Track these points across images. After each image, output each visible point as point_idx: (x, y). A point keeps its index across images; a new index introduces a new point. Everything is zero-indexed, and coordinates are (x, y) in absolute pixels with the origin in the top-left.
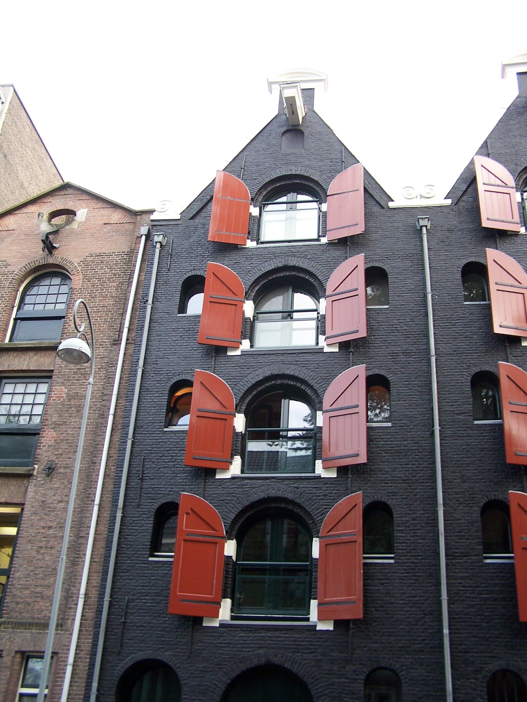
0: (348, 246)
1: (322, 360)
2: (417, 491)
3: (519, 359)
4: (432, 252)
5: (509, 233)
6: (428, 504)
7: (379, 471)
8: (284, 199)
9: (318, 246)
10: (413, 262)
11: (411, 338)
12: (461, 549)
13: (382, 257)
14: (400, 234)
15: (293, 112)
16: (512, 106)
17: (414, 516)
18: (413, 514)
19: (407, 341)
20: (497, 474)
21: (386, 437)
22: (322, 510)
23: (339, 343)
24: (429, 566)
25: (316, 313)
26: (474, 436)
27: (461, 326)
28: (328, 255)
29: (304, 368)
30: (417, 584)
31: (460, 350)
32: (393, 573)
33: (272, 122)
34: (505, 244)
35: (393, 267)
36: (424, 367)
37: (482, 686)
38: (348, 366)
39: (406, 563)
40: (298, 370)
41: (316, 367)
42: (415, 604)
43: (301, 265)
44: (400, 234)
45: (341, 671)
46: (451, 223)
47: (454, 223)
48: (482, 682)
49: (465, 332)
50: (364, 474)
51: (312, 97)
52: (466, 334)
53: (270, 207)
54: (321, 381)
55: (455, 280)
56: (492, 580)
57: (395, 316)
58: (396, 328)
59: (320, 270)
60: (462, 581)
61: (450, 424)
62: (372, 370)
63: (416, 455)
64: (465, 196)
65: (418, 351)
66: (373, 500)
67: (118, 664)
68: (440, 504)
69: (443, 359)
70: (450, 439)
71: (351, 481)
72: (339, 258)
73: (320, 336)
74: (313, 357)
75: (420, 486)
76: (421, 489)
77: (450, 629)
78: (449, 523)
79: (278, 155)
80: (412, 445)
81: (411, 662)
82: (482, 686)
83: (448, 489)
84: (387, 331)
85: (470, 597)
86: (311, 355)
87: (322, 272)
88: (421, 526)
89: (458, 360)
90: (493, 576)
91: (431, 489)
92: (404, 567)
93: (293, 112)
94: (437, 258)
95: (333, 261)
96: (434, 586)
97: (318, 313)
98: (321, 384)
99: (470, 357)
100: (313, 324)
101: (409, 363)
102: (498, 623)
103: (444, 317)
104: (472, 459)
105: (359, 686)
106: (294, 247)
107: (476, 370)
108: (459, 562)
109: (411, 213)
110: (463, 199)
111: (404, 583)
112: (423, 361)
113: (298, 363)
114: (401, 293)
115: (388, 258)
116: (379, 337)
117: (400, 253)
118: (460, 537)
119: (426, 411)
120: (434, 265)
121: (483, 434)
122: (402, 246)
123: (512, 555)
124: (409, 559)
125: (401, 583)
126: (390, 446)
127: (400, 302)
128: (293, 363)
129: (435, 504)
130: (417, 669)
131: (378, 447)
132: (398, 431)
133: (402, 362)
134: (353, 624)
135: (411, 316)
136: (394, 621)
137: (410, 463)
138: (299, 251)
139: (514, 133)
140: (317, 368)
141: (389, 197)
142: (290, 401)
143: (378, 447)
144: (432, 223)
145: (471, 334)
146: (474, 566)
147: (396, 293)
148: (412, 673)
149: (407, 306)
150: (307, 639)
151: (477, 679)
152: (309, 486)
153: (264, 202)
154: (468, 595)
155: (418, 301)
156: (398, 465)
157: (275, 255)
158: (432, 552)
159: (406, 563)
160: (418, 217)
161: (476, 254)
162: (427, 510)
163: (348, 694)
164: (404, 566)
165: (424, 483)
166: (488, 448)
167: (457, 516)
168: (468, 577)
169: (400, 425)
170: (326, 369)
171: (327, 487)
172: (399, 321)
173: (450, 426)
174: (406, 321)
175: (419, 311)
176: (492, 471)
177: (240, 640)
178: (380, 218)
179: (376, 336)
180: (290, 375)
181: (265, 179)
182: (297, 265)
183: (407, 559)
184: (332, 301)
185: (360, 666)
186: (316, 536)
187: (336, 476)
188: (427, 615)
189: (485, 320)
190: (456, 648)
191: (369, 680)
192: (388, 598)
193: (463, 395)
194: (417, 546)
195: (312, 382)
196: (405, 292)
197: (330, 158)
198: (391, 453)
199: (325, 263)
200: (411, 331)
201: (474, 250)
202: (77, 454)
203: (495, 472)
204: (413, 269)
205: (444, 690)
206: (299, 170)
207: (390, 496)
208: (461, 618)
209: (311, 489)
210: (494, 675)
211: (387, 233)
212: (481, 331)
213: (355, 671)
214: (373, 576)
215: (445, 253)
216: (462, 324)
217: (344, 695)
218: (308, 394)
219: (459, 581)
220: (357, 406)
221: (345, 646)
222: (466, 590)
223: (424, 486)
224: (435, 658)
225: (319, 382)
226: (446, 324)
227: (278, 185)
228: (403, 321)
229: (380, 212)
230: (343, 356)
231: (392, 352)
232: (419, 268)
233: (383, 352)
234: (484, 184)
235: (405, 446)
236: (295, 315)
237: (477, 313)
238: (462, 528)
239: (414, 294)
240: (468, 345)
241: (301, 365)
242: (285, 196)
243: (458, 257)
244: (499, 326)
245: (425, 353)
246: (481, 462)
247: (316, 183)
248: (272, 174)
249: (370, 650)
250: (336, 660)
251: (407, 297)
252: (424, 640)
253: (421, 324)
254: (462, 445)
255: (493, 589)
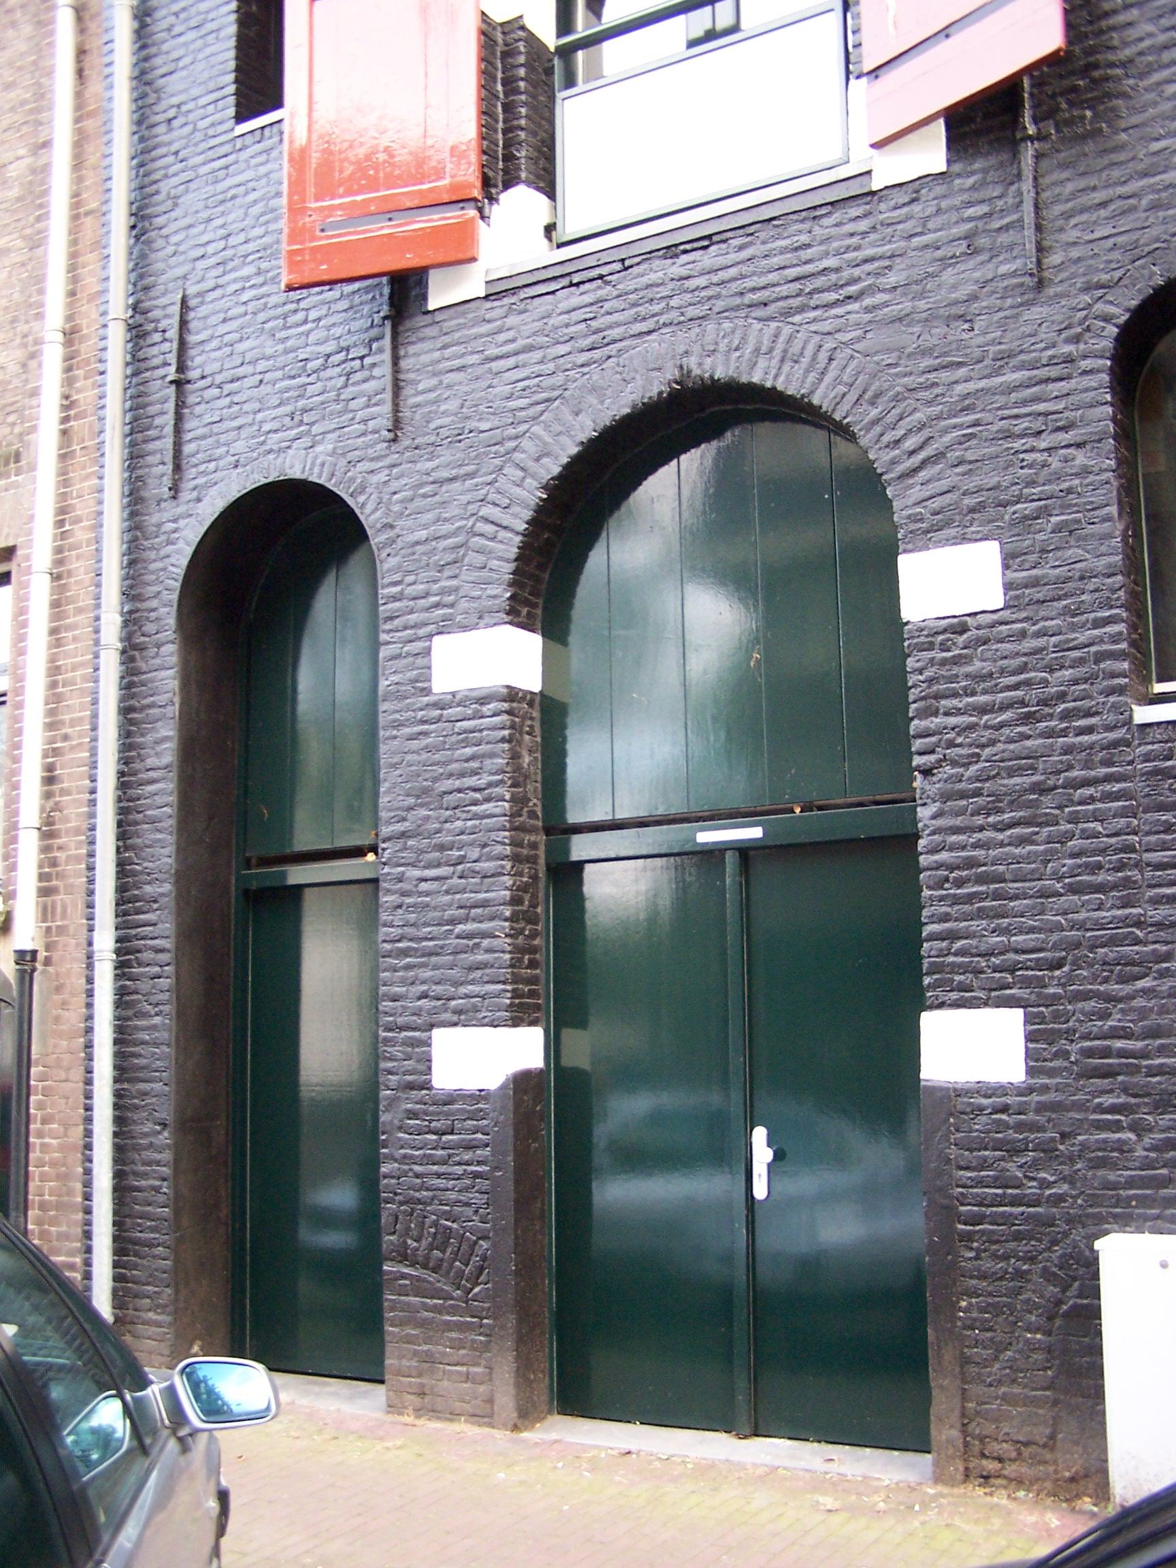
67: (175, 531)
150: (835, 244)
177: (567, 325)
202: (38, 473)
244: (1170, 1262)
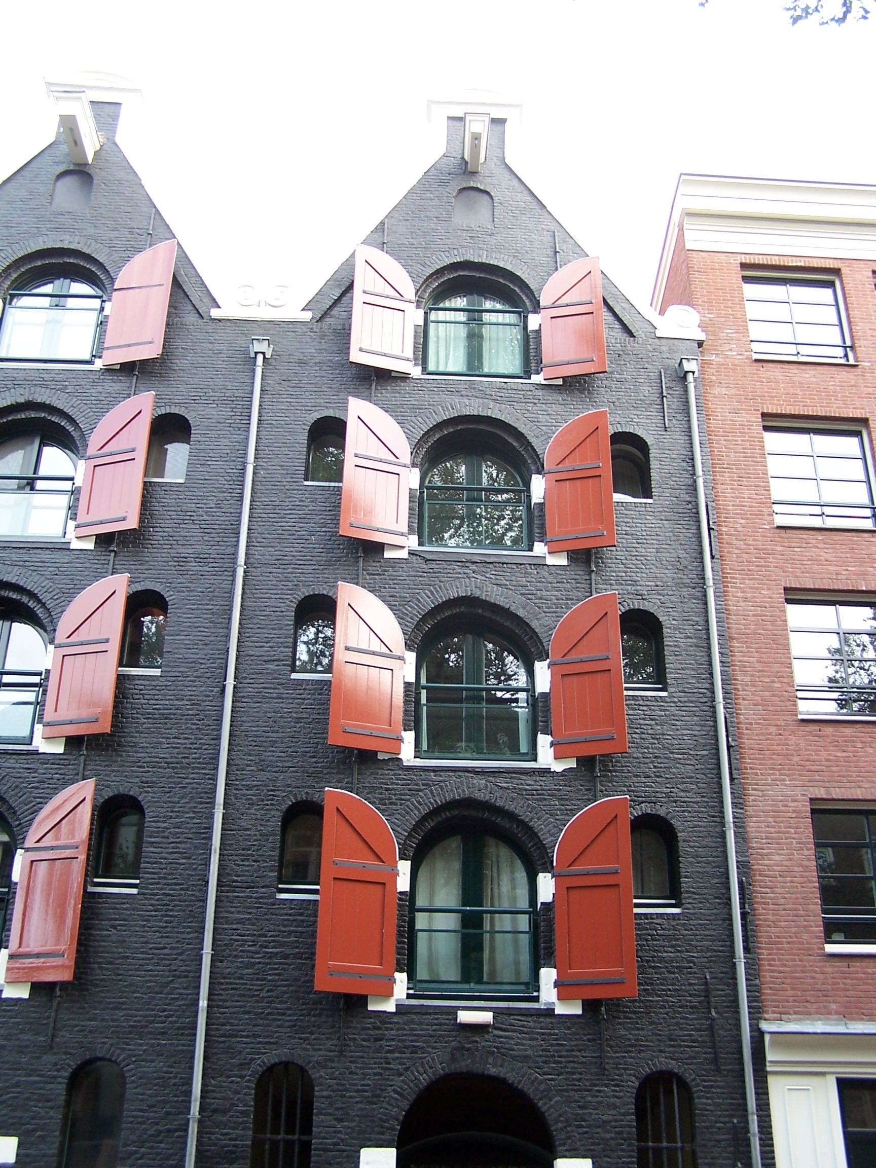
0: (135, 377)
1: (66, 561)
2: (187, 781)
3: (376, 579)
4: (267, 396)
5: (393, 374)
6: (201, 803)
7: (132, 746)
8: (48, 289)
9: (86, 373)
10: (234, 410)
11: (212, 535)
12: (244, 876)
13: (186, 399)
14: (221, 363)
15: (76, 143)
16: (433, 169)
17: (178, 820)
18: (177, 817)
19: (205, 538)
20: (315, 760)
21: (150, 692)
22: (34, 806)
23: (96, 535)
24: (191, 901)
25: (71, 482)
26: (287, 698)
27: (293, 520)
28: (100, 389)
29: (35, 573)
30: (169, 929)
31: (286, 558)
32: (133, 909)
33: (42, 155)
34: (384, 391)
35: (200, 417)
36: (226, 582)
37: (248, 1087)
38: (105, 574)
39: (156, 894)
40: (24, 576)
41: (55, 573)
42: (163, 959)
43: (55, 403)
44: (221, 363)
45: (32, 1064)
46: (305, 351)
47: (309, 351)
48: (248, 1081)
49: (299, 529)
50: (107, 750)
51: (115, 118)
52: (299, 533)
53: (25, 301)
54: (59, 595)
55: (297, 445)
56: (285, 926)
57: (193, 498)
58: (191, 516)
59: (84, 413)
60: (239, 926)
61: (253, 676)
62: (142, 583)
63: (192, 724)
64: (336, 309)
65: (220, 556)
66: (116, 793)
68: (219, 805)
69: (256, 572)
70: (250, 700)
71: (85, 761)
72: (118, 395)
73: (69, 521)
74: (52, 556)
75: (193, 773)
76: (194, 779)
77: (209, 1000)
78: (230, 834)
79: (44, 213)
80: (188, 707)
81: (145, 1051)
82: (248, 1087)
83: (236, 780)
84: (175, 521)
85: (249, 951)
86: (50, 553)
87: (87, 416)
88: (185, 838)
89: (280, 575)
90: (288, 920)
91: (209, 779)
92: (153, 902)
93: (76, 143)
94: (274, 408)
95: (108, 399)
96: (196, 932)
97: (74, 484)
98: (58, 601)
99: (300, 571)
100: (64, 500)
101: (202, 575)
102: (285, 992)
103: (270, 503)
104: (281, 735)
105: (59, 1089)
106: (48, 372)
107: (306, 592)
108: (238, 897)
109: (245, 329)
110: (332, 313)
111: (149, 927)
112: (225, 573)
113: (27, 563)
114: (208, 461)
115: (196, 401)
116: (161, 530)
117: (216, 394)
118: (243, 857)
119: (218, 654)
120: (267, 418)
121: (302, 696)
122: (222, 383)
123: (318, 887)
124: (161, 889)
125: (144, 926)
126: (154, 707)
127: (203, 475)
128: (18, 563)
129: (212, 803)
130: (152, 1061)
131: (135, 708)
132: (170, 683)
133: (192, 573)
134: (60, 990)
135: (217, 498)
136: (126, 986)
137: (182, 736)
138: (56, 379)
139: (428, 214)
140: (56, 575)
141: (214, 300)
142: (14, 625)
143: (135, 708)
144: (276, 349)
145: (308, 533)
146: (260, 903)
147: (200, 460)
148: (144, 1067)
149: (213, 482)
151: (242, 1077)
152: (18, 765)
153: (13, 290)
154: (246, 948)
155: (232, 475)
156: (163, 738)
157: (15, 382)
158: (199, 880)
159: (156, 894)
160: (253, 337)
161: (336, 405)
162: (198, 812)
163: (39, 1101)
164: (153, 899)
165: (199, 768)
166: (308, 718)
167: (244, 824)
168: (249, 919)
169: (174, 674)
170: (70, 577)
171: (46, 769)
172: (198, 505)
173: (253, 681)
174: (208, 506)
175: (231, 491)
176: (308, 755)
178: (194, 334)
179: (157, 527)
180: (11, 583)
181: (17, 251)
182: (48, 402)
183: (158, 889)
184: (95, 466)
185: (64, 1057)
186: (21, 846)
187: (62, 751)
188: (179, 977)
189: (333, 513)
190: (218, 1030)
191: (76, 1079)
192: (121, 950)
193: (281, 632)
194: (176, 869)
195: (44, 597)
196: (214, 459)
197: (130, 226)
198: (155, 719)
199: (94, 402)
200: (213, 522)
201: (335, 397)
203: (313, 757)
204: (233, 421)
205: (189, 1093)
206: (76, 242)
207: (144, 787)
208: (231, 983)
209: (21, 770)
210: (271, 1069)
211: (201, 360)
212: (323, 529)
213: (56, 1064)
214: (101, 914)
215: (288, 400)
216: (296, 516)
217: (32, 1103)
218: (37, 615)
219: (234, 927)
220: (107, 641)
221: (44, 1024)
222: (243, 940)
223: (200, 773)
224: (183, 1045)
225: (56, 597)
226: (271, 515)
227: (39, 263)
228: (204, 506)
229: (195, 323)
230: (99, 558)
231: (178, 555)
232: (242, 422)
233: (164, 555)
234: (365, 292)
235: (177, 709)
236: (40, 485)
237: (323, 500)
238: (250, 843)
239: (227, 463)
240: (301, 552)
241: (32, 568)
242: (50, 283)
243: (307, 408)
245: (229, 561)
246: (293, 740)
247: (101, 266)
248: (29, 245)
249: (84, 1031)
250: (27, 1046)
251: (215, 467)
252: (170, 1016)
253: (231, 513)
254: (266, 712)
255: (285, 940)
